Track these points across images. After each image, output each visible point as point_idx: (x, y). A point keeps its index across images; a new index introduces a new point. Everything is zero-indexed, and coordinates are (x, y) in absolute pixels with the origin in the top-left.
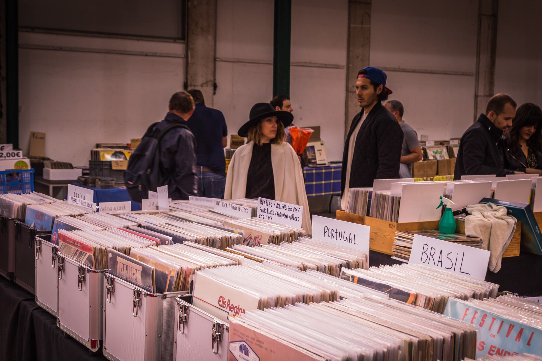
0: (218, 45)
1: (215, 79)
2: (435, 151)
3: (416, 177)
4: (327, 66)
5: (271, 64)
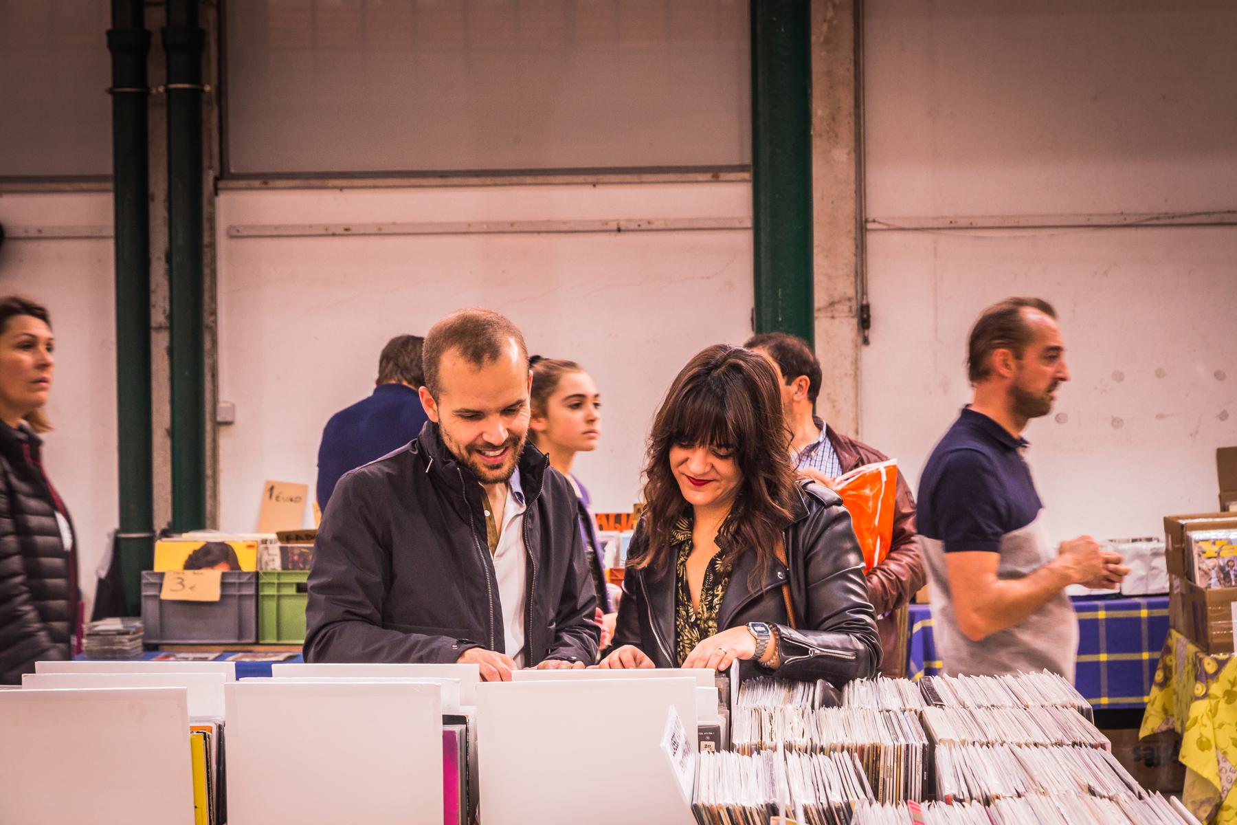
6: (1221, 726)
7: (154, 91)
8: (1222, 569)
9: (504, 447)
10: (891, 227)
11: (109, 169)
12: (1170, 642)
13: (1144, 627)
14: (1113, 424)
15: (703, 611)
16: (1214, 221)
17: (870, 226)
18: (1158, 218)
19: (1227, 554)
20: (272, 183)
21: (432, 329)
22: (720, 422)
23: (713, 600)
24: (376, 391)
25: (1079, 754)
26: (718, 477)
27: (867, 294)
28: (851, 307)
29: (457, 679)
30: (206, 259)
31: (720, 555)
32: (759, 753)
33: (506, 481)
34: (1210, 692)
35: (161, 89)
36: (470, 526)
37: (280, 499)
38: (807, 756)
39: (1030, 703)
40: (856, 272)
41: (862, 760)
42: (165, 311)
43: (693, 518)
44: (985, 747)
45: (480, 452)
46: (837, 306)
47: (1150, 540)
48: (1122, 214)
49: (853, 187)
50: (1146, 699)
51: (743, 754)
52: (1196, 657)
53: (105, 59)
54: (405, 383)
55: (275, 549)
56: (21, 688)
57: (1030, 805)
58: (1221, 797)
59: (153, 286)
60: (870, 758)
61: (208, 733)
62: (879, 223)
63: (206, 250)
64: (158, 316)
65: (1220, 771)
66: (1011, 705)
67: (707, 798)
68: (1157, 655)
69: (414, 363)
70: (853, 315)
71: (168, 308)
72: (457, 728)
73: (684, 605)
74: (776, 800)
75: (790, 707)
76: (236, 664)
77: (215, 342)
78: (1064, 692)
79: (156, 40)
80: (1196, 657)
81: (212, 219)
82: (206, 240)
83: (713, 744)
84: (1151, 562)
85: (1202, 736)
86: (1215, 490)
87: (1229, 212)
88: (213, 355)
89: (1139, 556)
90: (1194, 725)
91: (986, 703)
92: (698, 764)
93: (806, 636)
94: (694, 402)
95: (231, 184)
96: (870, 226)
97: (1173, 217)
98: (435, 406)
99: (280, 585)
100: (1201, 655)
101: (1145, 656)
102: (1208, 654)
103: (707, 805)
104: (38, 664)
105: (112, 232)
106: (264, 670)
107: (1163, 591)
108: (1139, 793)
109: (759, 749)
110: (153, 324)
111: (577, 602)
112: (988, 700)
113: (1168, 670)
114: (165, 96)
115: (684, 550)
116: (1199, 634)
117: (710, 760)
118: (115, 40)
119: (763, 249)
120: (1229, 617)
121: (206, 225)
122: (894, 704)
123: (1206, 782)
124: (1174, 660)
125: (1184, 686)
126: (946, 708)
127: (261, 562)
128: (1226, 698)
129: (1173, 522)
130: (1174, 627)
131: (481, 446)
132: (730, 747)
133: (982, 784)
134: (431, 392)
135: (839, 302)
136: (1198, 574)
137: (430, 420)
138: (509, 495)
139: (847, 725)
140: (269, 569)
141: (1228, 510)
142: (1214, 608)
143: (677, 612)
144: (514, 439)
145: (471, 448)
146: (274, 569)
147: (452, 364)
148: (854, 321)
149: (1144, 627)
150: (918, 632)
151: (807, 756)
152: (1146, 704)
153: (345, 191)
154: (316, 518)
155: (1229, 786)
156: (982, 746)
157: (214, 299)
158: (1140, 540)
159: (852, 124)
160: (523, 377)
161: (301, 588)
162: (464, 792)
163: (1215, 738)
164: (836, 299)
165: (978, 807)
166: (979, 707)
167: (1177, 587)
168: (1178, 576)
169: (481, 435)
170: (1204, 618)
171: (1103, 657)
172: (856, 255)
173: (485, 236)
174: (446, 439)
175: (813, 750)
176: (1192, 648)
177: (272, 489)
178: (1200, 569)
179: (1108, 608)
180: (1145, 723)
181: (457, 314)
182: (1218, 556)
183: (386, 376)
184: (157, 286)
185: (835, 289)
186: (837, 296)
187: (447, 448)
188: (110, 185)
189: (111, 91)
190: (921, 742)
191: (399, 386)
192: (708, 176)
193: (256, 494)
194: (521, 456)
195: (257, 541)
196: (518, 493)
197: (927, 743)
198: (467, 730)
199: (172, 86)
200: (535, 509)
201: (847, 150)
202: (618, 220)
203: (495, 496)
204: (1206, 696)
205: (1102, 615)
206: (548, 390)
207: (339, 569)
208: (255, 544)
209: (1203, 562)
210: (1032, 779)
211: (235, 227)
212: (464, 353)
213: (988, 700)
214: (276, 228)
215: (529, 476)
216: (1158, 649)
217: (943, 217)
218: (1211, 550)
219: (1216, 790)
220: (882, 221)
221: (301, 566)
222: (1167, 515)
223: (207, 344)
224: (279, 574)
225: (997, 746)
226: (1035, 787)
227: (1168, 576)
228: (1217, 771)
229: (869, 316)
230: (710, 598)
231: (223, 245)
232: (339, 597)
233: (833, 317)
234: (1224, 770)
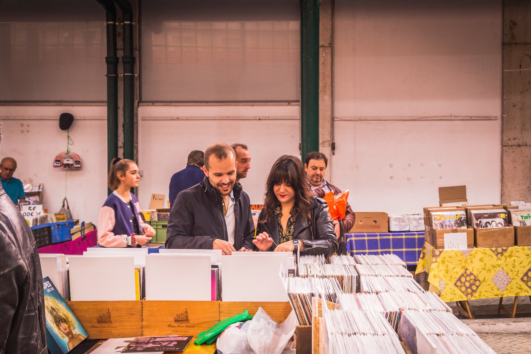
0: (337, 104)
1: (333, 139)
2: (526, 215)
3: (480, 246)
4: (473, 118)
5: (106, 120)
6: (440, 271)
7: (120, 76)
8: (441, 224)
9: (229, 184)
11: (106, 99)
12: (425, 245)
13: (417, 241)
14: (407, 180)
15: (287, 234)
18: (422, 118)
19: (442, 220)
20: (155, 104)
21: (207, 149)
22: (287, 177)
23: (290, 230)
24: (187, 167)
25: (404, 279)
26: (288, 194)
27: (334, 140)
28: (329, 143)
29: (216, 254)
30: (135, 127)
31: (291, 217)
32: (307, 278)
33: (229, 195)
34: (437, 261)
35: (122, 75)
36: (218, 208)
37: (156, 199)
38: (322, 278)
39: (388, 263)
40: (331, 133)
41: (338, 280)
42: (122, 142)
43: (281, 207)
44: (375, 276)
45: (221, 186)
46: (325, 143)
47: (418, 214)
48: (411, 116)
49: (330, 107)
50: (417, 262)
51: (302, 278)
52: (433, 250)
53: (105, 66)
54: (196, 165)
55: (156, 214)
56: (83, 256)
57: (390, 294)
58: (440, 292)
59: (119, 135)
60: (341, 279)
61: (140, 270)
63: (135, 124)
64: (120, 143)
65: (440, 284)
66: (382, 264)
67: (292, 291)
68: (420, 249)
69: (198, 159)
70: (329, 146)
71: (123, 141)
72: (216, 269)
73: (281, 232)
74: (314, 292)
75: (315, 264)
76: (148, 249)
77: (137, 152)
78: (398, 260)
79: (121, 60)
80: (433, 250)
81: (137, 115)
82: (135, 121)
83: (293, 275)
84: (419, 221)
85: (434, 274)
86: (438, 200)
87: (443, 116)
88: (137, 156)
89: (415, 219)
90: (432, 270)
91: (374, 263)
92: (289, 281)
93: (312, 242)
94: (278, 171)
95: (143, 104)
96: (335, 119)
98: (208, 172)
99: (157, 225)
100: (435, 249)
101: (417, 249)
102: (437, 249)
103: (292, 293)
104: (88, 249)
105: (106, 118)
106: (156, 251)
107: (423, 230)
108: (423, 291)
109: (307, 276)
110: (119, 146)
111: (250, 231)
112: (375, 262)
113: (424, 254)
114: (123, 77)
115: (279, 216)
116: (434, 243)
117: (293, 280)
118: (108, 60)
119: (304, 125)
120: (443, 238)
121: (135, 116)
122: (347, 263)
123: (436, 287)
124: (426, 250)
125: (429, 259)
126: (363, 265)
127: (151, 218)
128: (442, 262)
129: (426, 209)
130: (426, 241)
131: (221, 184)
132: (298, 275)
133: (375, 288)
134: (206, 168)
135: (326, 142)
136: (434, 225)
137: (206, 176)
138: (230, 199)
139: (333, 269)
140: (154, 220)
141: (442, 206)
142: (439, 235)
143: (279, 234)
144: (231, 182)
145: (218, 185)
146: (155, 220)
147: (213, 159)
148: (330, 148)
149: (417, 241)
150: (349, 241)
151: (322, 278)
152: (417, 264)
153: (177, 106)
154: (168, 205)
155: (443, 289)
156: (374, 276)
157: (137, 139)
158: (415, 215)
159: (330, 88)
160: (234, 163)
161: (164, 226)
162: (217, 289)
163: (439, 275)
164: (325, 141)
165: (375, 294)
166: (373, 264)
167: (427, 229)
168: (428, 225)
169: (221, 181)
170: (436, 238)
171: (404, 250)
172: (331, 128)
173: (219, 120)
174: (211, 182)
175: (323, 277)
176: (432, 247)
177: (154, 196)
178: (434, 223)
179: (406, 235)
180: (417, 270)
181: (214, 144)
182: (440, 220)
183: (190, 162)
184: (120, 134)
185: (325, 138)
186: (325, 140)
187: (211, 185)
188: (106, 104)
189: (107, 76)
190: (356, 275)
191: (194, 166)
192: (287, 104)
193: (149, 197)
194: (234, 187)
195: (150, 212)
196: (233, 198)
197: (358, 275)
198: (218, 270)
199: (125, 74)
200: (238, 203)
201: (329, 96)
202: (260, 116)
203: (225, 199)
204: (436, 262)
205: (404, 237)
206: (126, 169)
207: (175, 221)
208: (150, 213)
209: (435, 221)
210: (390, 286)
211: (144, 117)
212: (216, 156)
213: (375, 262)
214: (156, 117)
215: (236, 193)
216: (421, 248)
217: (357, 117)
218: (438, 218)
219: (439, 290)
220: (339, 118)
221: (164, 219)
222: (424, 207)
223: (135, 152)
224: (157, 222)
225: (379, 276)
226: (391, 289)
227: (424, 225)
228: (439, 284)
229: (335, 146)
230: (289, 229)
231: (140, 122)
232: (176, 229)
233: (324, 146)
234: (441, 284)
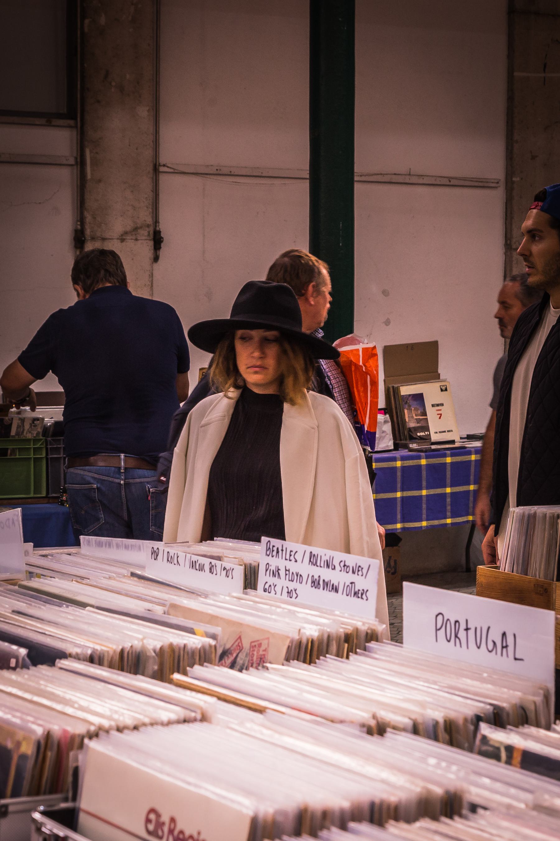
10: (176, 171)
16: (386, 180)
17: (162, 169)
28: (149, 232)
62: (168, 167)
97: (361, 176)
135: (141, 227)
192: (43, 121)
201: (148, 108)
233: (136, 240)
